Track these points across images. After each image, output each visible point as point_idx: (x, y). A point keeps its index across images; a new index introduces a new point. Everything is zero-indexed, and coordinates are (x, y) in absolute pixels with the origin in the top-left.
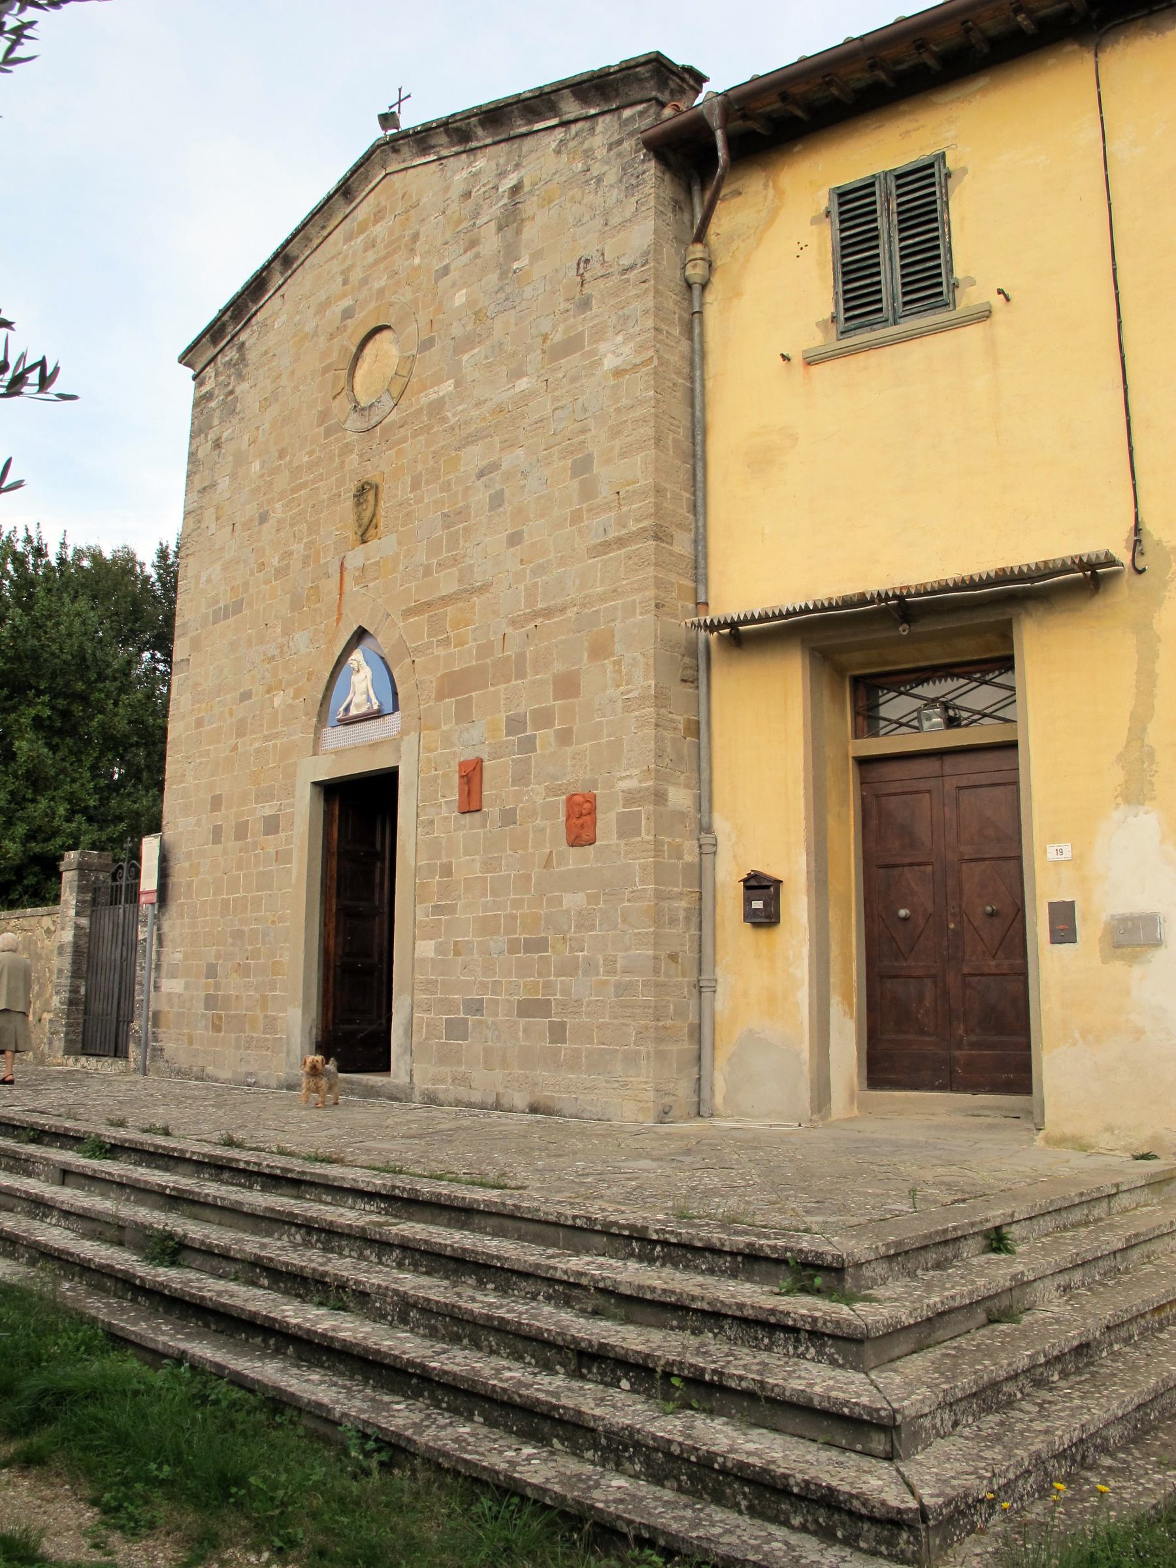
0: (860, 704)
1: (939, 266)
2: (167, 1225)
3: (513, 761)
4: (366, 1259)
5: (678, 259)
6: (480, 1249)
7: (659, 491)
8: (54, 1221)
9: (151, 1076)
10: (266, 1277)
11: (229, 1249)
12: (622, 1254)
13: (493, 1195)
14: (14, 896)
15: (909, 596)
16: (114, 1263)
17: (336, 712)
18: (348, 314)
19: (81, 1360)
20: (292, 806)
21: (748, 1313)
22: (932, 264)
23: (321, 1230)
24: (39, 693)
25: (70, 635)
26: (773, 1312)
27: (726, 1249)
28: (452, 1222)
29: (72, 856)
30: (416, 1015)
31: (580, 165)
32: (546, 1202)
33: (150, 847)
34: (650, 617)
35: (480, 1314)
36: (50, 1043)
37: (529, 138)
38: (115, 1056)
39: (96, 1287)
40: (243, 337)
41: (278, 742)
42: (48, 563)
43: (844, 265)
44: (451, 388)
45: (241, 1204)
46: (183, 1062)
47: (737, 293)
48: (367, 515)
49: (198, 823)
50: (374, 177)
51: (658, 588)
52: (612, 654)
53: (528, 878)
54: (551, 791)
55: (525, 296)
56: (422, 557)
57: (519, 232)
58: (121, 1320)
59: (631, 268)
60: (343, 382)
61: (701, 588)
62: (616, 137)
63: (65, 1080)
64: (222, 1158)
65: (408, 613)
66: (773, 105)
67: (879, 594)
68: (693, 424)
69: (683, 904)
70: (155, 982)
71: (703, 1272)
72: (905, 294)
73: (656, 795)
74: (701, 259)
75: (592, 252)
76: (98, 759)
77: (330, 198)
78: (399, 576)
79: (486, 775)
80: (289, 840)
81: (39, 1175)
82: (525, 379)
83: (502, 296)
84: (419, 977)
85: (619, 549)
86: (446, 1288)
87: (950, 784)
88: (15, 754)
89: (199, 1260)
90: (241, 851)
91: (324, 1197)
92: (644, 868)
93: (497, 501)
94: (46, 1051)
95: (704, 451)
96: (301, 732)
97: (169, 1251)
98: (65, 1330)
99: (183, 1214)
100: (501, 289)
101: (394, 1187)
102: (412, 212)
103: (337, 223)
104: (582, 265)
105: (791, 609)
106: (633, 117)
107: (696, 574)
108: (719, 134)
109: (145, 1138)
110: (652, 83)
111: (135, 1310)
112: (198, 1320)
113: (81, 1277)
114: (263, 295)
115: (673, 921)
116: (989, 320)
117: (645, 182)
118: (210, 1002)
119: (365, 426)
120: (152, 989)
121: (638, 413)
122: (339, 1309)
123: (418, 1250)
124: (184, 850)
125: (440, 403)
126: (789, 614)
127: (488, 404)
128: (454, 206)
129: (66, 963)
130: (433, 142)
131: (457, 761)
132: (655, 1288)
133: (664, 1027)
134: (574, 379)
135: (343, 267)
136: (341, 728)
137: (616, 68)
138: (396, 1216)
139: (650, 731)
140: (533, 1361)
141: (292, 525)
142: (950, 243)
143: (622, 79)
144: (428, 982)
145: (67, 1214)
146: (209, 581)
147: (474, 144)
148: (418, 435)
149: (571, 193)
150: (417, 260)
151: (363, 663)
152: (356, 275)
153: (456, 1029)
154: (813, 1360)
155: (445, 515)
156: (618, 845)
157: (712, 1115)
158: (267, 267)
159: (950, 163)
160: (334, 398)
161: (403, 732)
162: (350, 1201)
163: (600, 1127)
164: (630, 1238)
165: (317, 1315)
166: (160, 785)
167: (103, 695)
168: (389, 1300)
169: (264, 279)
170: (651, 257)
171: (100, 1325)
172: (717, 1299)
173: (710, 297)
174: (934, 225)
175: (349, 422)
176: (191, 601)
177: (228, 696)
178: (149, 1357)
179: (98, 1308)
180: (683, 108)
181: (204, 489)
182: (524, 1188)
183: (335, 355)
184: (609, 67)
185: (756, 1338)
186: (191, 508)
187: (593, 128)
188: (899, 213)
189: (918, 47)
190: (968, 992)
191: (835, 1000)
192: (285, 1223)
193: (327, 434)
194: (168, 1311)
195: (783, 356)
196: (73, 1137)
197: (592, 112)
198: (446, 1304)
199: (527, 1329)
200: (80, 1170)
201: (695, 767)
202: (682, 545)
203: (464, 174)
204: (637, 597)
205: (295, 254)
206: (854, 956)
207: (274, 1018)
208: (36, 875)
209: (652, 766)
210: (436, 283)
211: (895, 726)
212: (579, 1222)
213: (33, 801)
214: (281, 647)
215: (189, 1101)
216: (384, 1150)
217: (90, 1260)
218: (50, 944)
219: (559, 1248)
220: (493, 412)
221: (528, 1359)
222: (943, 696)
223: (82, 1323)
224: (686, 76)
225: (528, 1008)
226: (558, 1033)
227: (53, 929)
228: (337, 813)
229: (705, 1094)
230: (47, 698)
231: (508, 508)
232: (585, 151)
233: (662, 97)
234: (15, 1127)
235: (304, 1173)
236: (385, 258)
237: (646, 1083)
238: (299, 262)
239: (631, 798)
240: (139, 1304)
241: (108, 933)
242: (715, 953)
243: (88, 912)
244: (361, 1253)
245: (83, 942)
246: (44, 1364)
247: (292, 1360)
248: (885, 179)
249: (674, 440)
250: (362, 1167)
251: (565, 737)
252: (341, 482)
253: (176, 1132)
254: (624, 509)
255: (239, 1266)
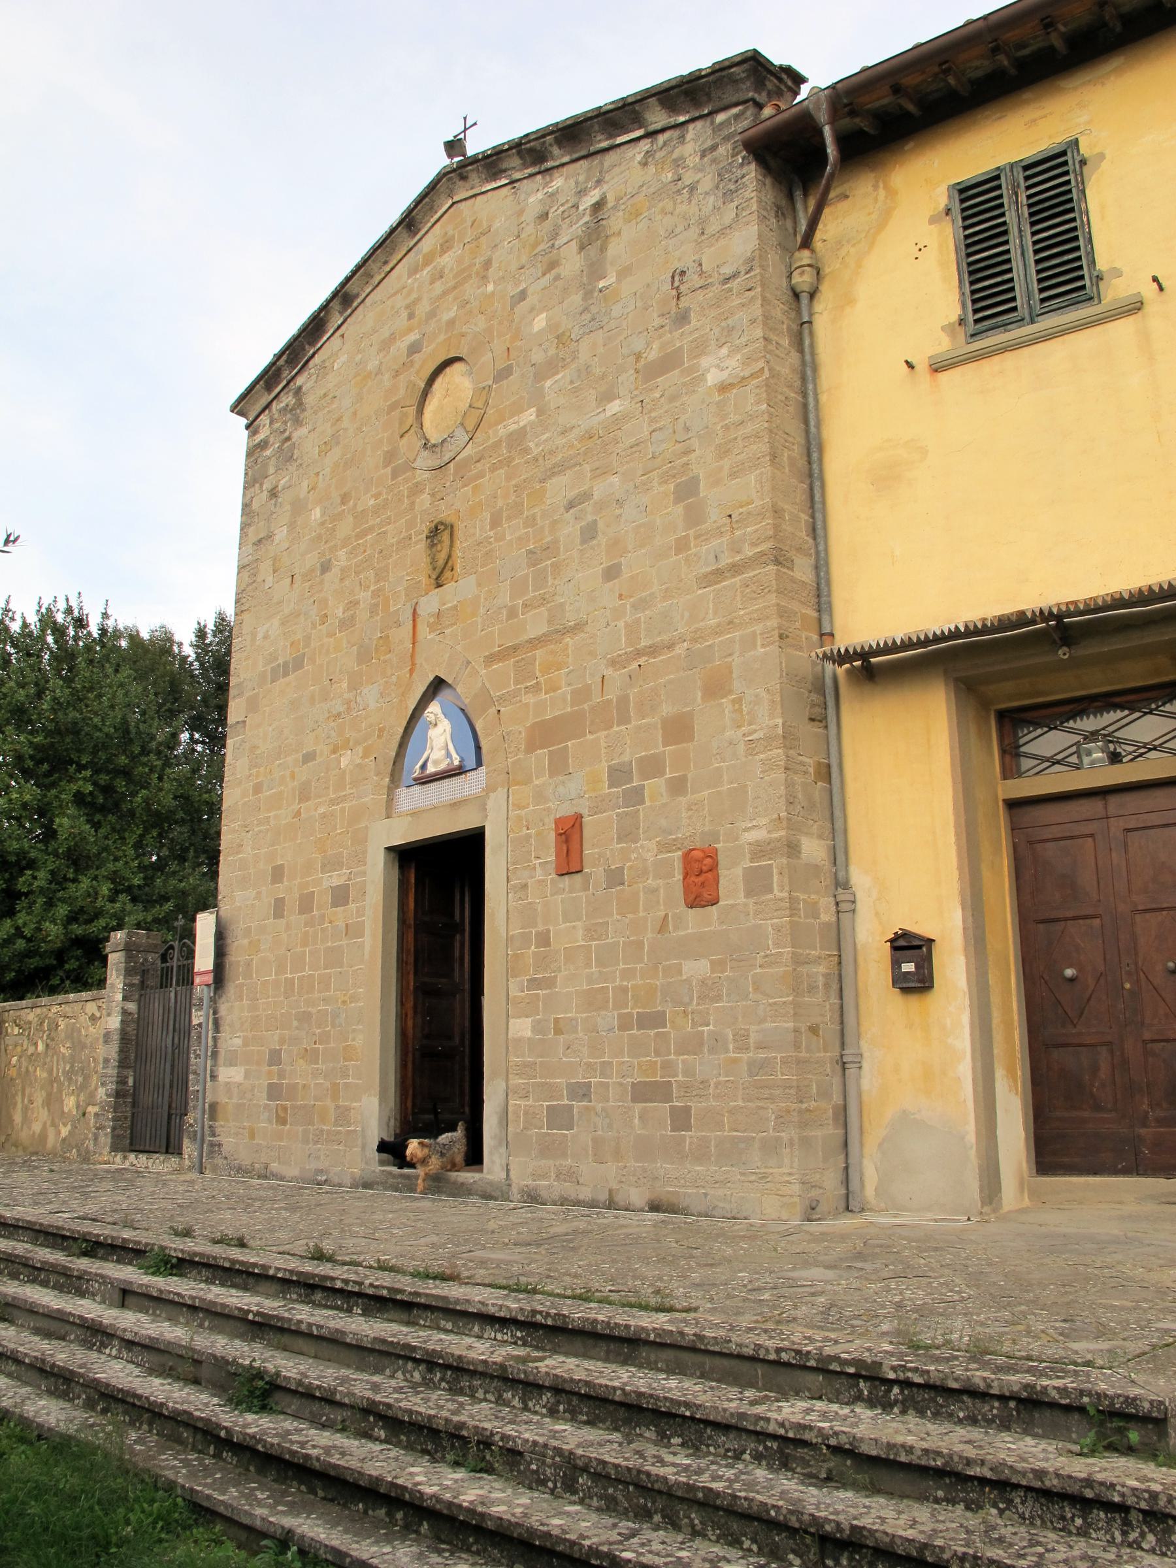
0: (1006, 742)
1: (1079, 258)
2: (254, 1360)
3: (618, 815)
4: (507, 1403)
5: (783, 268)
6: (661, 1393)
7: (777, 512)
8: (114, 1352)
9: (208, 1174)
10: (382, 1428)
11: (334, 1392)
12: (845, 1397)
13: (660, 1321)
14: (56, 981)
15: (1070, 615)
16: (191, 1408)
17: (411, 771)
18: (414, 349)
19: (160, 1541)
20: (364, 873)
21: (1051, 1483)
22: (1071, 256)
23: (447, 1367)
24: (81, 768)
25: (112, 707)
26: (1088, 1482)
27: (995, 1391)
28: (611, 1356)
29: (119, 936)
30: (511, 1102)
31: (670, 175)
32: (732, 1329)
33: (205, 924)
34: (774, 648)
35: (677, 1483)
36: (96, 1139)
37: (611, 153)
38: (167, 1152)
39: (169, 1438)
40: (299, 381)
41: (347, 805)
42: (90, 634)
43: (969, 264)
44: (533, 417)
45: (344, 1333)
46: (244, 1158)
47: (849, 300)
48: (442, 557)
49: (258, 896)
50: (440, 207)
51: (781, 617)
52: (730, 692)
53: (640, 945)
54: (664, 847)
55: (614, 314)
56: (505, 598)
57: (603, 249)
58: (205, 1485)
59: (734, 276)
60: (411, 419)
61: (825, 618)
62: (709, 143)
63: (114, 1179)
64: (314, 1276)
65: (491, 659)
66: (883, 99)
67: (1041, 611)
68: (808, 442)
69: (822, 969)
70: (212, 1071)
71: (960, 1421)
72: (1041, 290)
73: (789, 847)
74: (809, 265)
75: (688, 263)
76: (142, 836)
77: (393, 231)
78: (479, 620)
79: (587, 832)
80: (360, 912)
81: (94, 1295)
82: (617, 402)
83: (587, 316)
84: (513, 1059)
85: (734, 576)
86: (620, 1444)
87: (1116, 827)
88: (55, 832)
89: (295, 1405)
90: (306, 926)
91: (443, 1323)
92: (778, 929)
93: (589, 533)
94: (91, 1147)
95: (821, 471)
96: (372, 794)
97: (258, 1393)
98: (137, 1499)
99: (270, 1345)
100: (586, 309)
101: (534, 1312)
102: (483, 239)
103: (400, 257)
104: (677, 278)
105: (938, 633)
106: (728, 121)
107: (819, 603)
108: (827, 131)
109: (217, 1250)
110: (748, 84)
111: (220, 1470)
112: (301, 1483)
113: (150, 1424)
114: (321, 336)
115: (812, 989)
116: (1140, 314)
117: (745, 185)
118: (274, 1091)
119: (437, 463)
120: (208, 1079)
121: (749, 428)
122: (480, 1471)
123: (578, 1394)
124: (242, 926)
125: (521, 433)
126: (937, 639)
127: (576, 431)
128: (530, 230)
129: (112, 1051)
130: (504, 166)
131: (552, 818)
132: (912, 1447)
133: (807, 1110)
134: (673, 399)
135: (407, 301)
136: (417, 788)
137: (709, 71)
138: (537, 1348)
139: (780, 776)
140: (755, 1548)
141: (357, 573)
142: (1090, 233)
143: (715, 82)
144: (526, 1065)
145: (130, 1344)
146: (266, 637)
147: (549, 164)
148: (497, 469)
149: (661, 204)
150: (490, 288)
151: (441, 716)
152: (423, 308)
153: (560, 1117)
154: (1152, 1551)
155: (531, 552)
156: (746, 905)
157: (863, 1210)
158: (325, 307)
159: (1084, 149)
160: (402, 436)
161: (490, 789)
162: (476, 1328)
163: (739, 1227)
164: (857, 1376)
165: (456, 1481)
166: (214, 858)
167: (147, 770)
168: (549, 1461)
169: (322, 319)
170: (756, 263)
171: (179, 1491)
172: (1004, 1464)
173: (818, 307)
174: (1071, 216)
175: (419, 460)
176: (247, 658)
177: (289, 759)
178: (243, 1536)
179: (174, 1467)
180: (783, 107)
181: (260, 541)
182: (695, 1310)
183: (402, 392)
184: (700, 70)
185: (1063, 1518)
186: (246, 561)
187: (683, 136)
188: (1030, 206)
189: (1046, 26)
190: (1150, 1059)
191: (1000, 1074)
192: (399, 1356)
193: (395, 474)
194: (261, 1471)
195: (907, 362)
196: (132, 1250)
197: (682, 119)
198: (629, 1469)
199: (746, 1504)
200: (144, 1290)
201: (827, 814)
202: (803, 571)
203: (540, 195)
204: (758, 628)
205: (355, 292)
206: (1016, 1023)
207: (348, 1109)
208: (78, 959)
209: (783, 814)
210: (512, 309)
211: (1048, 764)
212: (785, 1356)
213: (75, 881)
214: (349, 702)
215: (257, 1204)
216: (502, 1261)
217: (162, 1404)
218: (94, 1032)
219: (759, 1390)
220: (581, 439)
221: (747, 1544)
222: (1103, 729)
223: (156, 1489)
224: (784, 76)
225: (644, 1092)
226: (681, 1119)
227: (98, 1015)
228: (413, 881)
229: (854, 1184)
230: (88, 773)
231: (602, 540)
232: (675, 160)
233: (761, 98)
234: (64, 1237)
235: (417, 1294)
236: (455, 288)
237: (790, 1174)
238: (359, 300)
239: (760, 850)
240: (224, 1460)
241: (158, 1018)
242: (858, 1024)
243: (137, 997)
244: (500, 1396)
245: (131, 1029)
246: (113, 1550)
247: (429, 1542)
248: (1012, 171)
249: (789, 456)
250: (484, 1285)
251: (678, 786)
252: (411, 524)
253: (252, 1243)
254: (738, 533)
255: (347, 1413)
